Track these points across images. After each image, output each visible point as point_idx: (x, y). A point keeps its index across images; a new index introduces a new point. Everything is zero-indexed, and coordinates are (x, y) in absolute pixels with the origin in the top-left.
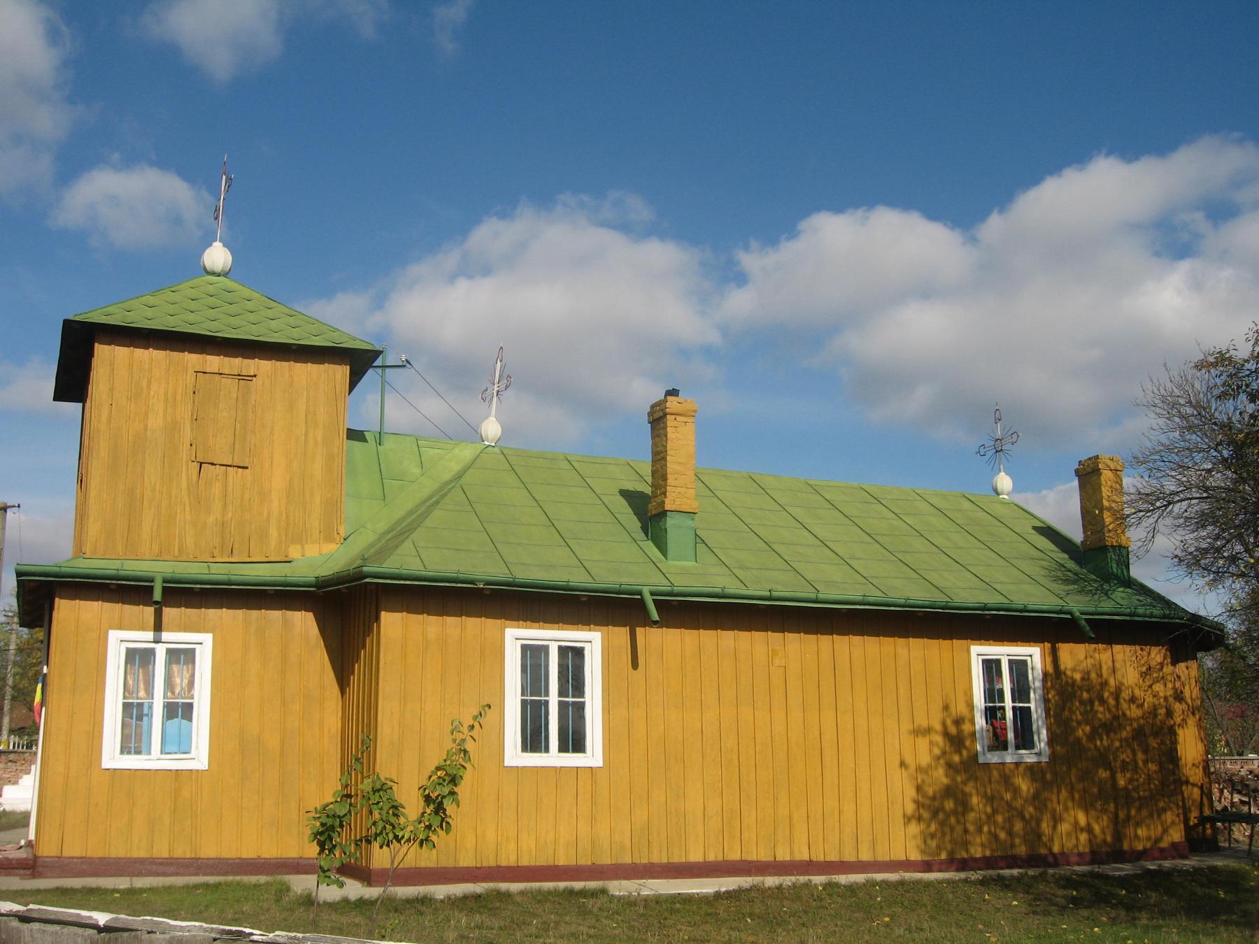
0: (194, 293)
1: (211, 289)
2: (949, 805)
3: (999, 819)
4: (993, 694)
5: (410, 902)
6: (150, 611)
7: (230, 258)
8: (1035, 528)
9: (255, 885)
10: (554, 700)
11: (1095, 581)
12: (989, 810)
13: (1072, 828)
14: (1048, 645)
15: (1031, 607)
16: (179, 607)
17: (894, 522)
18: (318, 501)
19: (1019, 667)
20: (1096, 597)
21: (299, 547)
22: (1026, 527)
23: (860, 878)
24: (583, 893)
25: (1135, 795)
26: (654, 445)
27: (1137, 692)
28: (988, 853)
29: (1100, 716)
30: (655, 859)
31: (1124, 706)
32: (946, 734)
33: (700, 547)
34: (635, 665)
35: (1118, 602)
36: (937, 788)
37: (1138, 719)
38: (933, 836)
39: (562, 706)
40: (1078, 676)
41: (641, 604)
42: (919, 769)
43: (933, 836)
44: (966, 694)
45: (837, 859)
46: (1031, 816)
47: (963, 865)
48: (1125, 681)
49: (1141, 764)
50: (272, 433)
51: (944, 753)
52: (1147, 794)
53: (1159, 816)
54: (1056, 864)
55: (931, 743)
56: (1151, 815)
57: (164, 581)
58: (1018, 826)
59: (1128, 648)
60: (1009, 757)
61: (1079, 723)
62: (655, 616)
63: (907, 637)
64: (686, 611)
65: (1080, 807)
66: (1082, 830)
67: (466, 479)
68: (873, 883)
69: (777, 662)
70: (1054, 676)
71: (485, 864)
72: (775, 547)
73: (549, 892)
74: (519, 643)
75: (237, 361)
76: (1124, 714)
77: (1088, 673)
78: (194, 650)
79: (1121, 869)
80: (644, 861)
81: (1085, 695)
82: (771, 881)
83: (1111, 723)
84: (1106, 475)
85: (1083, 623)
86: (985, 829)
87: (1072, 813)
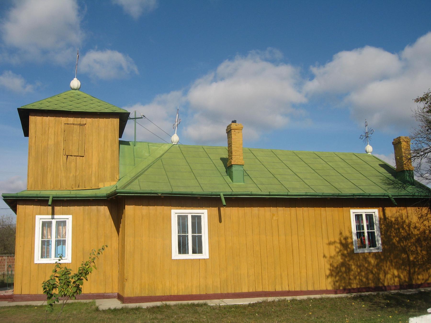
0: (65, 96)
1: (72, 95)
2: (343, 269)
3: (363, 274)
4: (359, 227)
5: (132, 309)
6: (50, 208)
7: (79, 84)
8: (380, 165)
9: (85, 304)
10: (190, 235)
11: (401, 183)
12: (359, 270)
13: (392, 276)
14: (381, 208)
15: (372, 194)
16: (60, 206)
17: (324, 165)
18: (109, 166)
19: (370, 217)
20: (400, 190)
21: (103, 183)
22: (376, 165)
23: (305, 297)
24: (198, 305)
25: (417, 263)
26: (228, 141)
27: (417, 225)
28: (359, 287)
29: (402, 234)
30: (230, 291)
31: (412, 230)
32: (341, 243)
33: (246, 178)
34: (220, 221)
35: (410, 191)
36: (338, 264)
37: (418, 235)
38: (337, 281)
39: (193, 237)
40: (393, 220)
41: (220, 199)
42: (331, 257)
43: (337, 281)
44: (348, 228)
45: (299, 290)
46: (376, 272)
47: (349, 291)
48: (412, 221)
49: (419, 251)
50: (92, 143)
51: (340, 251)
52: (422, 263)
53: (427, 271)
54: (386, 290)
55: (335, 247)
56: (424, 271)
57: (53, 198)
58: (371, 276)
59: (413, 208)
60: (366, 251)
61: (394, 237)
62: (224, 203)
63: (325, 207)
64: (235, 201)
65: (395, 268)
66: (396, 277)
67: (163, 157)
68: (309, 299)
69: (274, 218)
70: (384, 219)
71: (166, 295)
72: (297, 174)
73: (185, 305)
74: (177, 215)
75: (79, 119)
76: (412, 233)
77: (397, 218)
78: (66, 221)
79: (411, 291)
80: (225, 292)
81: (396, 226)
82: (270, 299)
83: (407, 236)
84: (404, 144)
85: (393, 199)
86: (358, 277)
87: (392, 270)
